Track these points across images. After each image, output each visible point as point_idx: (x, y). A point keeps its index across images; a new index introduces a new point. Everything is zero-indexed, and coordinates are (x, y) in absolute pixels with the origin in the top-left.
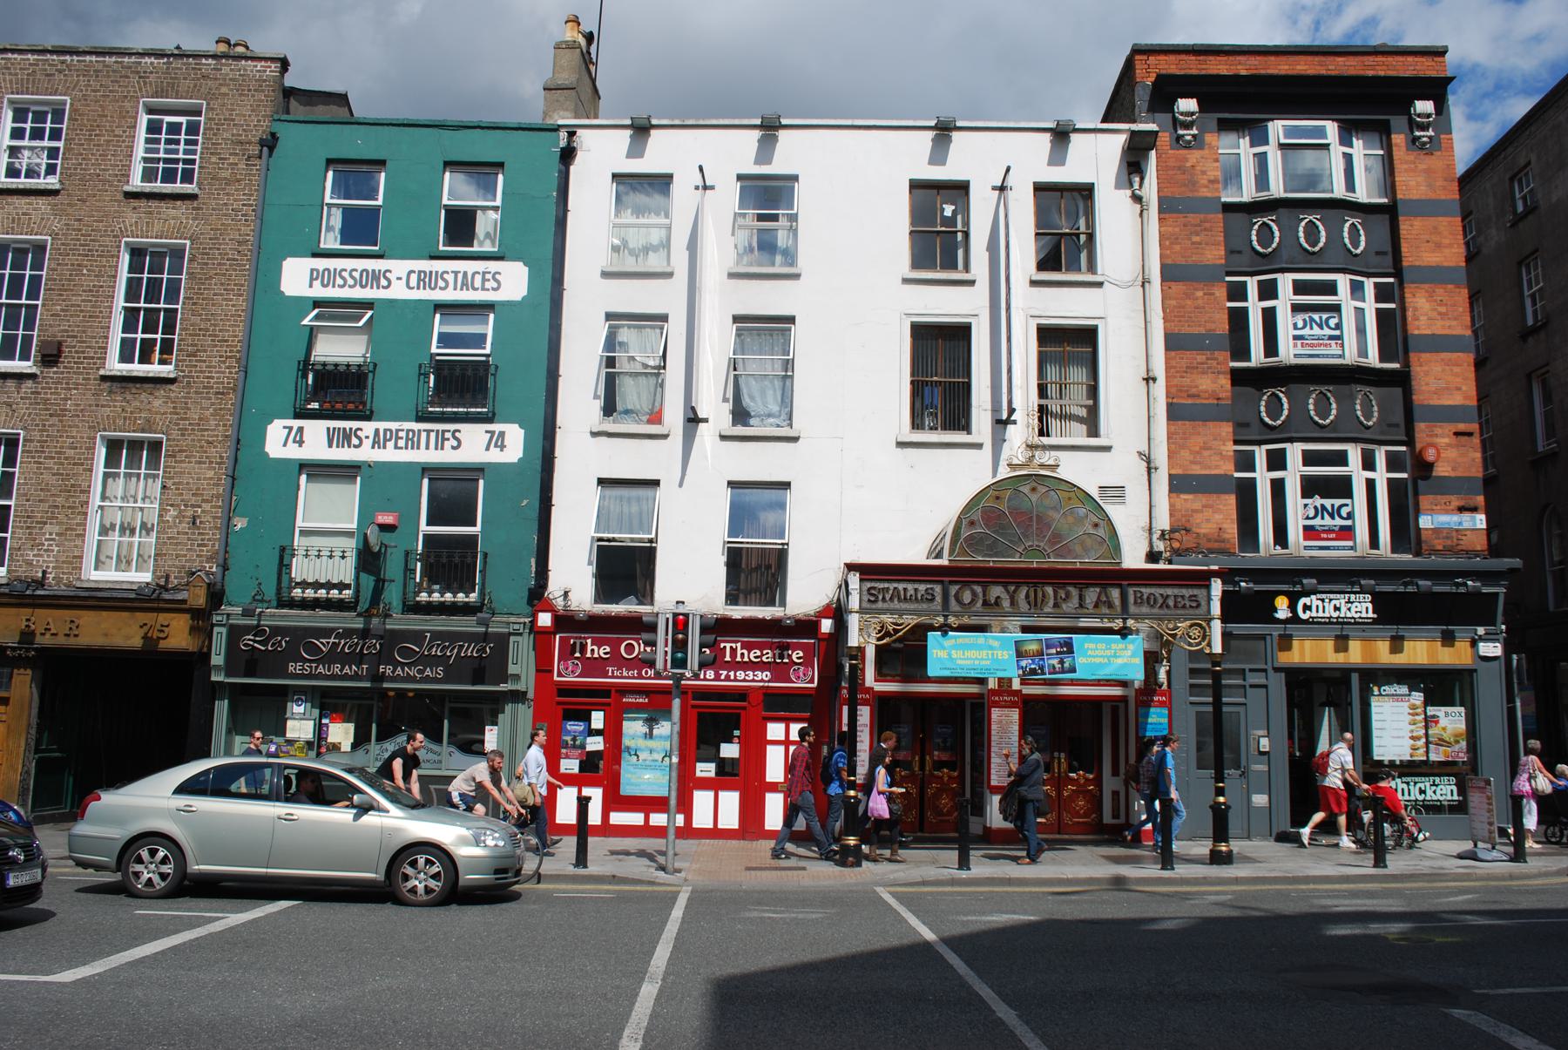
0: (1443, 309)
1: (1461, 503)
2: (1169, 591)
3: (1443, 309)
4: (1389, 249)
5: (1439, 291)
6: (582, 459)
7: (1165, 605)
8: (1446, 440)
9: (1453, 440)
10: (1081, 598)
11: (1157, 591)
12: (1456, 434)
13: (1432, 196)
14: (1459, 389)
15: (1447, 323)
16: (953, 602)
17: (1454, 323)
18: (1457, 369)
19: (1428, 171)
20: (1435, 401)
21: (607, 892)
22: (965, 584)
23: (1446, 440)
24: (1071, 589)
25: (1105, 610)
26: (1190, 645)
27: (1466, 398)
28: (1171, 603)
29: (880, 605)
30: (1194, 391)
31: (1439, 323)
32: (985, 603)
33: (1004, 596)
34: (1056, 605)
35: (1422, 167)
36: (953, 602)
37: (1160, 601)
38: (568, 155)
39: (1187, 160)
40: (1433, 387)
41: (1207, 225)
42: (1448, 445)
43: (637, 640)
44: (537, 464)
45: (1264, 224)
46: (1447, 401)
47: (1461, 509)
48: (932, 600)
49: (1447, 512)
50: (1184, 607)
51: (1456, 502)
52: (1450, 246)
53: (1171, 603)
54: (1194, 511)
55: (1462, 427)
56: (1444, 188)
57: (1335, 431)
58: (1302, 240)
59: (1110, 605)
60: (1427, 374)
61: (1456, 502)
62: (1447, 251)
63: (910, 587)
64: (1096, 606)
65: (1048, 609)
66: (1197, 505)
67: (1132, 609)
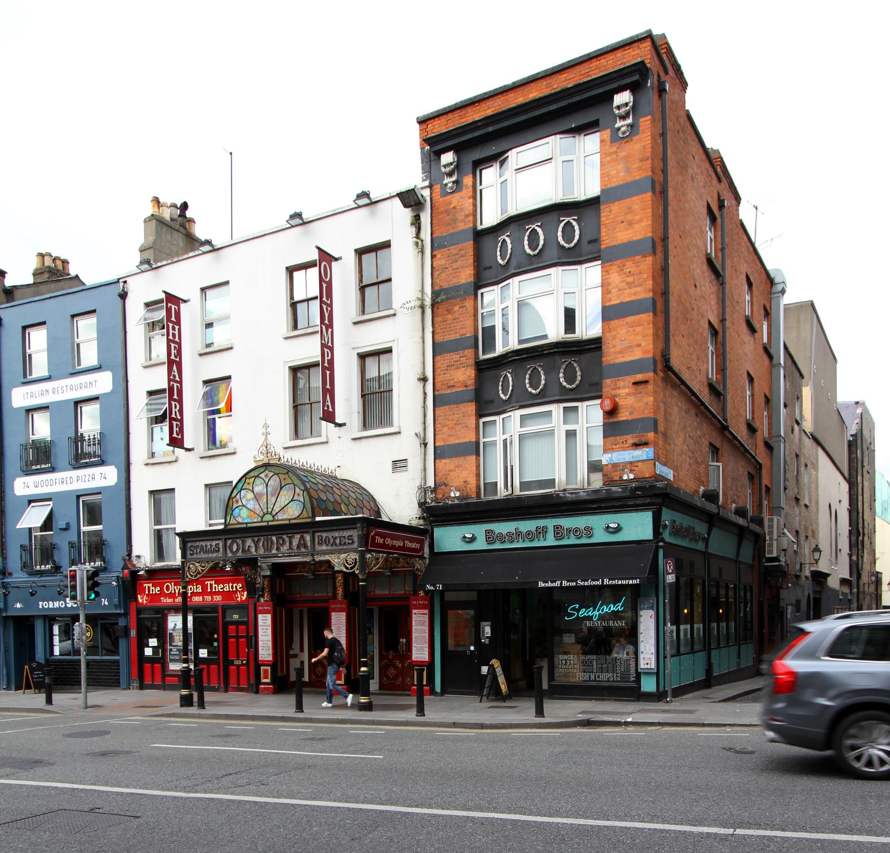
0: (630, 279)
1: (636, 440)
2: (337, 534)
3: (630, 279)
4: (380, 280)
5: (629, 264)
6: (144, 481)
7: (334, 544)
8: (627, 391)
9: (632, 389)
10: (291, 543)
11: (330, 535)
12: (635, 383)
13: (629, 179)
14: (639, 345)
15: (633, 290)
16: (228, 551)
17: (638, 289)
18: (638, 329)
19: (627, 157)
20: (620, 360)
21: (251, 725)
22: (234, 540)
23: (627, 391)
24: (284, 537)
25: (303, 550)
26: (347, 568)
27: (644, 352)
28: (338, 541)
29: (195, 556)
30: (451, 383)
31: (628, 291)
32: (243, 551)
33: (253, 545)
34: (278, 549)
35: (623, 154)
36: (228, 551)
37: (332, 540)
38: (123, 296)
39: (451, 203)
40: (618, 349)
41: (463, 252)
42: (628, 394)
43: (171, 583)
44: (123, 485)
45: (569, 222)
46: (628, 358)
47: (637, 445)
48: (218, 551)
49: (624, 449)
50: (345, 544)
51: (631, 439)
52: (641, 220)
53: (338, 541)
54: (450, 471)
55: (639, 377)
56: (640, 169)
57: (544, 397)
58: (560, 239)
59: (306, 547)
60: (614, 338)
61: (631, 439)
62: (636, 226)
63: (208, 543)
64: (298, 547)
65: (274, 551)
66: (452, 466)
67: (318, 548)
